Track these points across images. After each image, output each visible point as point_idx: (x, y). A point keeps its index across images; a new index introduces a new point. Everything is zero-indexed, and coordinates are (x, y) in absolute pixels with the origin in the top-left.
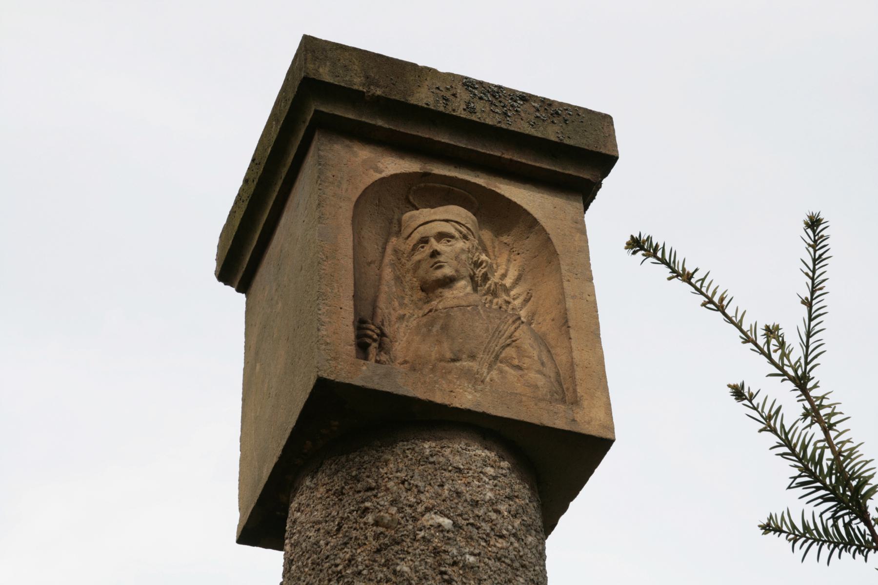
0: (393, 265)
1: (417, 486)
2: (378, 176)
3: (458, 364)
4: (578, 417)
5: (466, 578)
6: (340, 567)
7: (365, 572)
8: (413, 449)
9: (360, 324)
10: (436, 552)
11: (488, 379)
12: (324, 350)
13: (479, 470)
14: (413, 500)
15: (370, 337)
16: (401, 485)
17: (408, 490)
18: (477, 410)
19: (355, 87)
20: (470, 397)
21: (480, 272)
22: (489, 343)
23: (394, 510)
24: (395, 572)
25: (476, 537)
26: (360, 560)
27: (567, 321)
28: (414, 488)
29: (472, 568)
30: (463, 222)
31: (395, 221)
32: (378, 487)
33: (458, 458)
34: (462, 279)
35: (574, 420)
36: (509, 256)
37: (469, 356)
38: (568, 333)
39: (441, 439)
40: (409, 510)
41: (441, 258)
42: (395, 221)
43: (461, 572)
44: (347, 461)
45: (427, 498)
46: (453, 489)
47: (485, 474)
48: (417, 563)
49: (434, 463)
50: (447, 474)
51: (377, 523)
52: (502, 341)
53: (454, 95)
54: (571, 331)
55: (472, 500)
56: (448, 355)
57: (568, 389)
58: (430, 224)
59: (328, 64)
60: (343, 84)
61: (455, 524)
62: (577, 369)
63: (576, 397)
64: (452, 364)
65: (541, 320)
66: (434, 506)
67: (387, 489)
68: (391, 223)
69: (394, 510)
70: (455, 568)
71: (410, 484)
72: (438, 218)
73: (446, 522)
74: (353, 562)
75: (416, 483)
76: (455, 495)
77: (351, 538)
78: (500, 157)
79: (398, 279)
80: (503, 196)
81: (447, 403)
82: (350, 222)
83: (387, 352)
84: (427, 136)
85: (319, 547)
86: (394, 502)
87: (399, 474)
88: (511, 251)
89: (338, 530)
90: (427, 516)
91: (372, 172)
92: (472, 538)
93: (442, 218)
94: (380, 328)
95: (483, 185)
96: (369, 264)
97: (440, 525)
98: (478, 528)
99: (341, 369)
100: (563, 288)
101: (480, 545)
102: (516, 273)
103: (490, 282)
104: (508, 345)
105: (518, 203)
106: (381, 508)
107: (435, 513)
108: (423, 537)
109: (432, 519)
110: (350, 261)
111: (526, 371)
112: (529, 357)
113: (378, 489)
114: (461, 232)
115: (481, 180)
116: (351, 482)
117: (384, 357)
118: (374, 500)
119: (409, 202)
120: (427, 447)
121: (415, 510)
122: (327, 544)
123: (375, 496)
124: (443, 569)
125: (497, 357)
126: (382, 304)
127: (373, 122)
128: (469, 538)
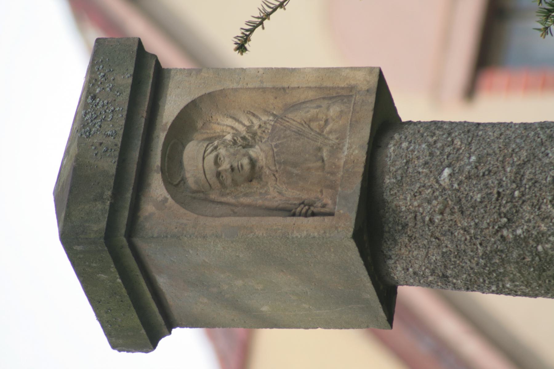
1: (419, 188)
3: (325, 159)
4: (365, 88)
5: (486, 162)
6: (468, 237)
7: (477, 221)
8: (391, 189)
10: (469, 178)
11: (337, 141)
13: (406, 151)
14: (430, 190)
15: (307, 211)
16: (417, 198)
17: (420, 193)
19: (107, 207)
20: (357, 152)
21: (239, 141)
22: (308, 138)
23: (435, 202)
24: (481, 202)
25: (457, 155)
26: (466, 224)
28: (420, 190)
29: (479, 158)
30: (204, 149)
31: (194, 195)
32: (415, 212)
33: (397, 163)
35: (368, 91)
38: (294, 88)
39: (383, 172)
40: (437, 193)
41: (235, 165)
42: (194, 195)
43: (482, 164)
44: (389, 232)
45: (429, 182)
46: (422, 166)
47: (408, 148)
48: (476, 189)
49: (402, 177)
50: (410, 170)
51: (442, 213)
53: (101, 144)
54: (292, 86)
55: (430, 156)
56: (319, 164)
57: (337, 93)
58: (206, 170)
59: (87, 224)
60: (107, 215)
61: (449, 166)
62: (325, 85)
63: (347, 88)
64: (326, 162)
65: (271, 107)
66: (435, 178)
67: (419, 206)
68: (194, 198)
69: (435, 202)
70: (480, 168)
71: (416, 192)
73: (447, 172)
74: (467, 229)
75: (417, 188)
76: (427, 166)
77: (449, 230)
78: (146, 119)
79: (246, 195)
80: (174, 121)
81: (363, 165)
85: (447, 252)
86: (429, 202)
87: (408, 199)
88: (210, 122)
89: (439, 239)
90: (442, 183)
91: (167, 204)
92: (458, 158)
95: (165, 133)
97: (450, 175)
98: (450, 154)
99: (344, 224)
100: (254, 88)
101: (461, 153)
103: (247, 136)
104: (309, 126)
106: (432, 210)
107: (440, 177)
108: (458, 185)
109: (444, 179)
111: (329, 117)
112: (317, 114)
113: (416, 212)
114: (212, 151)
115: (160, 137)
116: (406, 230)
117: (319, 204)
118: (424, 214)
119: (177, 185)
120: (388, 180)
121: (437, 189)
122: (446, 247)
123: (422, 214)
124: (481, 174)
125: (320, 134)
128: (458, 159)
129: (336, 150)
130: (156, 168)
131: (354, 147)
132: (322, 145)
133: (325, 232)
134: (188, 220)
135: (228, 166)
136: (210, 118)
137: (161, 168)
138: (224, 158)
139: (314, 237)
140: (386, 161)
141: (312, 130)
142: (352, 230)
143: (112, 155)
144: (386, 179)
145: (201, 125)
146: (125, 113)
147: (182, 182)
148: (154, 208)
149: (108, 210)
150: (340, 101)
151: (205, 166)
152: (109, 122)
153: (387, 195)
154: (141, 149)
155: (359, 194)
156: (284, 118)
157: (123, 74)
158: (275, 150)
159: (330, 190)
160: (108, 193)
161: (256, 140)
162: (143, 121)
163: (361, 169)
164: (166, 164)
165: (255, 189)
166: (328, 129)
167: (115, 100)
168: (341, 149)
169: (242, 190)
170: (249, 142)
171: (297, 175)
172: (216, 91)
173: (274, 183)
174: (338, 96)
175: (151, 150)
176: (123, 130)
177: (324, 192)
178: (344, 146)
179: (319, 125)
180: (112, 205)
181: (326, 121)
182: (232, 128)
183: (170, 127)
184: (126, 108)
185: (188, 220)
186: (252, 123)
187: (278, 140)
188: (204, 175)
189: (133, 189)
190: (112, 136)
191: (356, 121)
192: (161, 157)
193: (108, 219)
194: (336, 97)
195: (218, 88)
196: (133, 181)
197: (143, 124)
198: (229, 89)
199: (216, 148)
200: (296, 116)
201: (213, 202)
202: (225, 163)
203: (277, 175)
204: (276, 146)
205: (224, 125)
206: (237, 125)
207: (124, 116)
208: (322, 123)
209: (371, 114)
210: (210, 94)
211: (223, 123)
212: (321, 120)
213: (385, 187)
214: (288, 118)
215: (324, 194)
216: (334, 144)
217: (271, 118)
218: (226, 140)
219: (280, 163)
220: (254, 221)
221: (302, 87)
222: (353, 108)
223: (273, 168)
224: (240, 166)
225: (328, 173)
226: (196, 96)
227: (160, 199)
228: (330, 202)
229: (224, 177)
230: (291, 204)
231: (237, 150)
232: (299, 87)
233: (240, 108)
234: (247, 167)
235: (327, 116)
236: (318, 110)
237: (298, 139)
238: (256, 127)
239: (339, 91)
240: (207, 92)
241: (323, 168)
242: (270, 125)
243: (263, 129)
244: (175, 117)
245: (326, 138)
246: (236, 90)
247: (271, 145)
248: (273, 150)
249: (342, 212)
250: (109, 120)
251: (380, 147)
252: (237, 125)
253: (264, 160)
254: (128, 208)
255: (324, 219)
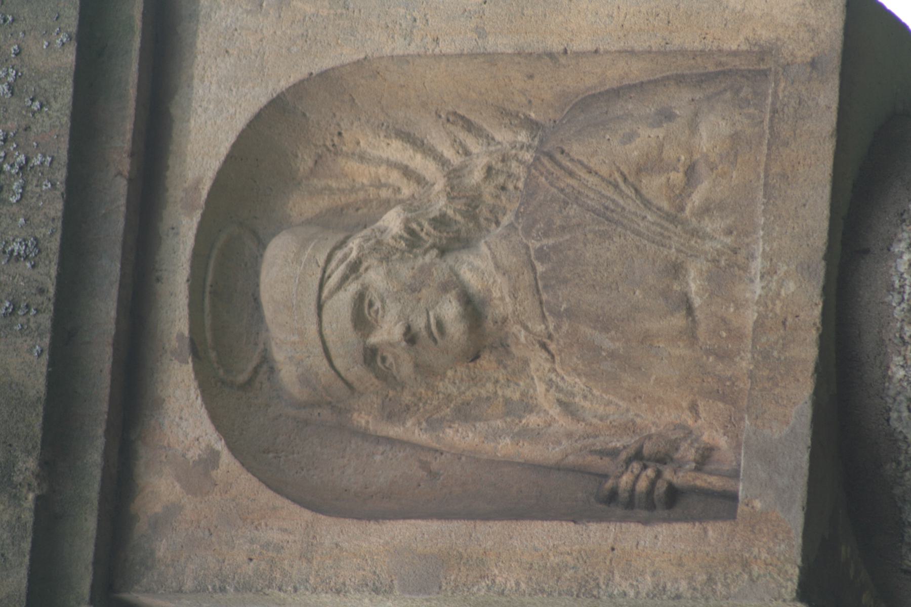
0: (434, 424)
2: (226, 458)
3: (697, 302)
4: (804, 53)
9: (613, 503)
11: (729, 240)
12: (727, 586)
15: (653, 484)
18: (822, 273)
19: (28, 517)
20: (792, 286)
22: (638, 234)
27: (551, 55)
34: (457, 275)
36: (347, 155)
37: (676, 277)
38: (578, 55)
39: (881, 343)
41: (419, 323)
52: (631, 206)
54: (576, 46)
56: (678, 321)
58: (330, 345)
60: (27, 546)
62: (677, 42)
64: (699, 315)
72: (313, 328)
78: (130, 181)
79: (465, 413)
81: (814, 335)
82: (372, 526)
83: (675, 445)
84: (109, 350)
88: (336, 152)
91: (218, 474)
93: (314, 319)
94: (628, 462)
96: (433, 475)
99: (769, 551)
102: (396, 144)
103: (450, 212)
105: (232, 139)
110: (482, 527)
111: (697, 156)
112: (661, 147)
114: (345, 279)
115: (182, 231)
117: (687, 452)
119: (249, 382)
125: (672, 219)
126: (552, 453)
127: (97, 473)
129: (725, 274)
130: (175, 344)
131: (783, 269)
132: (682, 257)
133: (710, 580)
134: (285, 531)
135: (397, 332)
136: (336, 139)
137: (192, 340)
138: (383, 301)
139: (678, 597)
140: (889, 304)
141: (647, 203)
142: (794, 572)
143: (33, 325)
144: (894, 369)
145: (310, 163)
146: (61, 175)
147: (265, 368)
148: (178, 486)
149: (30, 525)
150: (728, 95)
151: (327, 331)
152: (15, 209)
153: (900, 419)
154: (122, 286)
155: (809, 443)
156: (559, 156)
157: (48, 33)
158: (540, 268)
159: (721, 405)
160: (28, 464)
161: (482, 220)
162: (121, 187)
163: (807, 351)
164: (208, 322)
165: (490, 386)
166: (697, 198)
167: (28, 128)
168: (745, 269)
169: (453, 390)
170: (458, 231)
171: (612, 355)
172: (343, 66)
173: (548, 366)
174: (724, 73)
175: (158, 280)
176: (58, 236)
177: (701, 409)
178: (751, 257)
179: (669, 186)
180: (41, 503)
181: (691, 171)
182: (407, 172)
183: (209, 195)
184: (63, 155)
185: (285, 531)
186: (467, 153)
187: (546, 235)
188: (325, 361)
189: (107, 432)
190: (26, 258)
191: (784, 176)
192: (191, 305)
193: (32, 560)
194: (717, 74)
195: (347, 54)
196: (104, 407)
197: (123, 201)
198: (382, 58)
199: (355, 268)
200: (595, 153)
201: (364, 435)
202: (388, 318)
203: (552, 347)
204: (542, 255)
205: (380, 161)
206: (418, 162)
207: (61, 187)
208: (677, 177)
209: (828, 148)
210: (324, 75)
211: (375, 153)
212: (675, 169)
213: (892, 392)
214: (572, 160)
215: (703, 415)
216: (720, 253)
217: (523, 137)
218: (383, 231)
219: (557, 315)
220: (489, 534)
221: (607, 52)
222: (771, 127)
223: (539, 328)
224: (434, 328)
225: (708, 352)
226: (283, 84)
227: (194, 454)
228: (722, 442)
229: (390, 359)
230: (602, 453)
231: (422, 269)
232: (596, 51)
233: (424, 105)
234: (456, 329)
235: (691, 154)
236: (660, 132)
237: (604, 236)
238: (477, 176)
239: (724, 59)
240: (316, 70)
241: (690, 335)
242: (521, 162)
243: (501, 179)
244: (222, 158)
245: (694, 233)
246: (404, 59)
247: (527, 248)
248: (534, 269)
249: (758, 504)
250: (13, 200)
251: (867, 251)
252: (418, 162)
253: (508, 299)
254: (96, 503)
255: (705, 531)
